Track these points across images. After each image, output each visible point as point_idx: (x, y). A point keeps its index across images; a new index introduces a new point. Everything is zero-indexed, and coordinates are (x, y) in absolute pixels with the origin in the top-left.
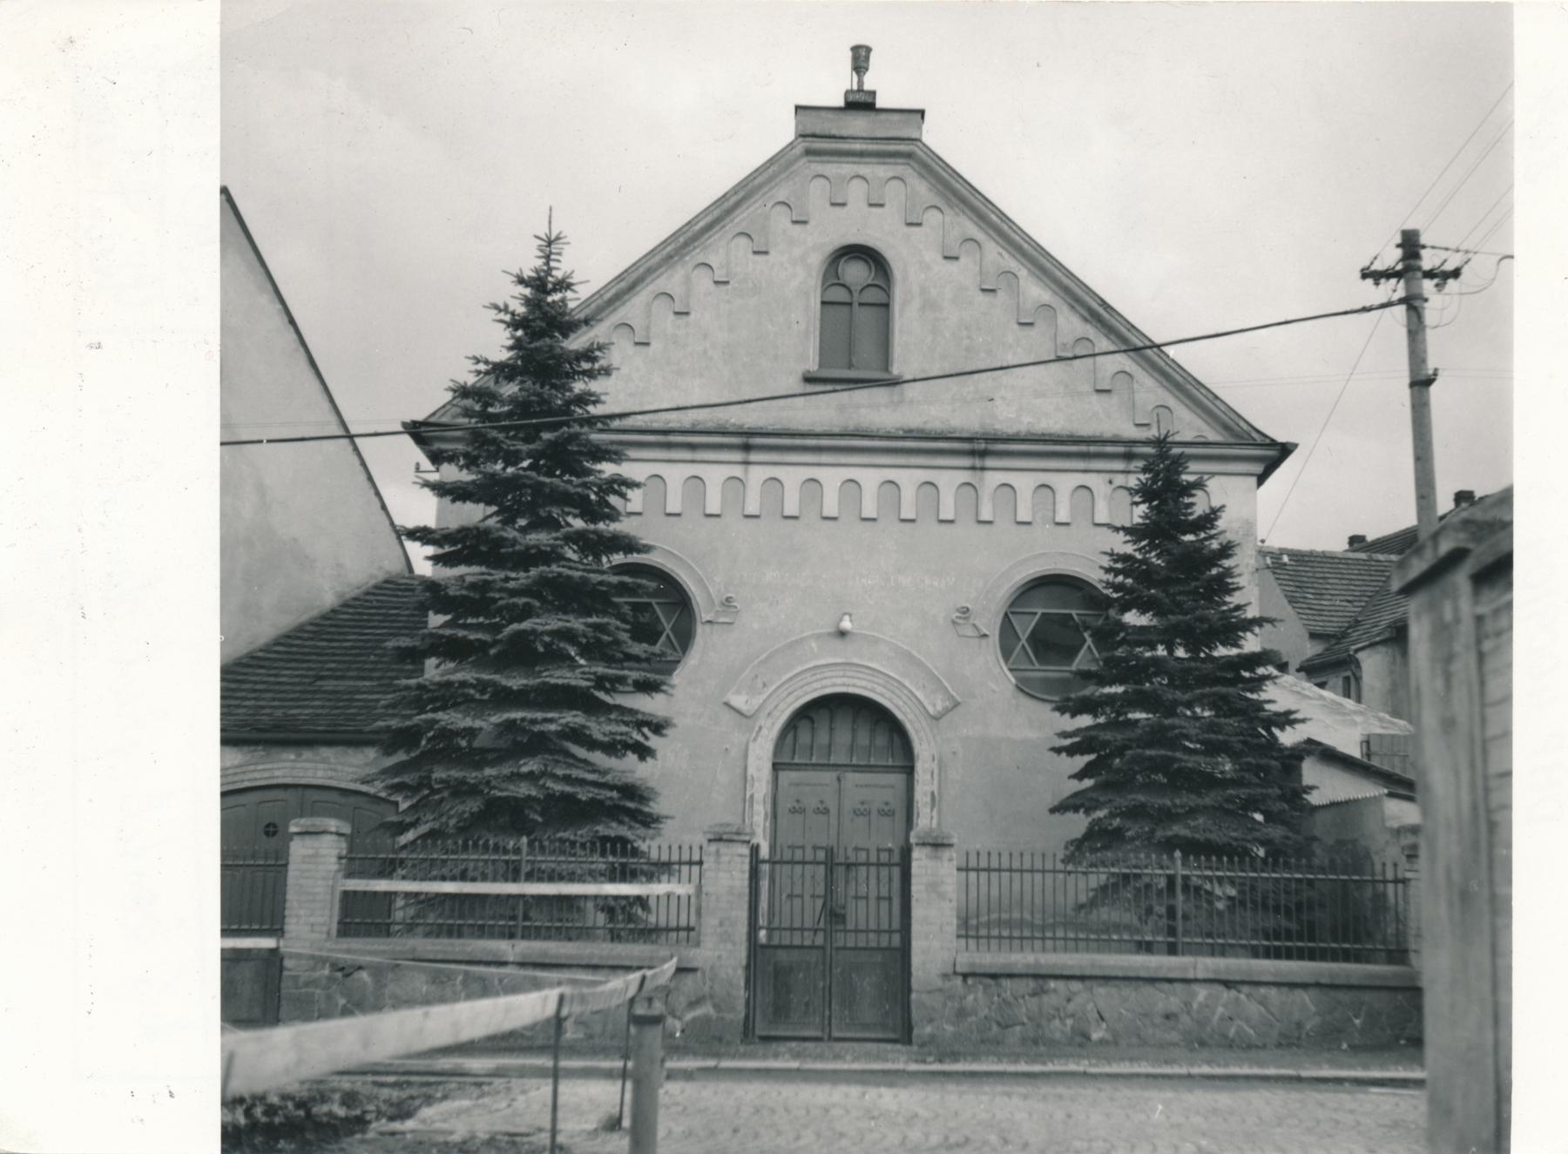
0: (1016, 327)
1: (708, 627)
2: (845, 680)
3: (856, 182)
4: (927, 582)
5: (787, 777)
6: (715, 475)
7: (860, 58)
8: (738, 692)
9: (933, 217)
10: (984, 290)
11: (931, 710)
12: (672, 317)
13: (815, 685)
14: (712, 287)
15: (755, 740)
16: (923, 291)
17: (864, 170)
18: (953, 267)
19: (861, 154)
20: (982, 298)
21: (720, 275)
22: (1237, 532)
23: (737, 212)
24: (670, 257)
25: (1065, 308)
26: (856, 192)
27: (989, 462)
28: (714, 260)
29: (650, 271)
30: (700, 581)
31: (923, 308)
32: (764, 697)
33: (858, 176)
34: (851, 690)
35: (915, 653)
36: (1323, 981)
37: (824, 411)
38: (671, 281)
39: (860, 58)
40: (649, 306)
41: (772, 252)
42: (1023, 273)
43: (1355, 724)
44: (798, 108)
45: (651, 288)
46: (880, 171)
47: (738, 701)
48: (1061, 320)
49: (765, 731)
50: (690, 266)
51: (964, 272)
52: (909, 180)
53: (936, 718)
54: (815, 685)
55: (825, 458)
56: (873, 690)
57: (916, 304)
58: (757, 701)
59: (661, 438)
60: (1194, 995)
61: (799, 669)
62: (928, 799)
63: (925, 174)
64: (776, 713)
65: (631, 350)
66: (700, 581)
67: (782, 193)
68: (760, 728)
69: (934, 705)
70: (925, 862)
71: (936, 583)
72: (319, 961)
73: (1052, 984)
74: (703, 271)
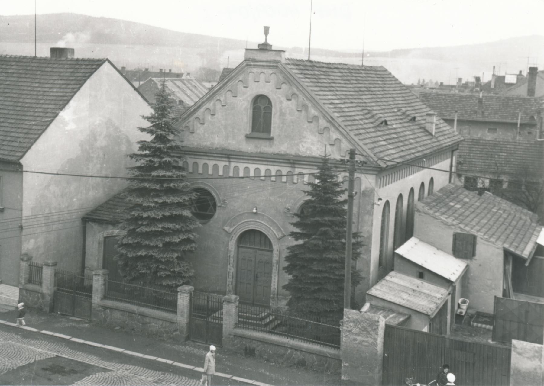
0: (307, 122)
1: (219, 208)
2: (255, 226)
3: (262, 74)
4: (278, 199)
5: (241, 250)
6: (221, 164)
7: (266, 30)
8: (227, 226)
9: (284, 86)
10: (298, 111)
11: (278, 236)
12: (210, 116)
13: (247, 227)
14: (221, 107)
15: (231, 240)
16: (281, 110)
17: (265, 70)
18: (289, 103)
19: (263, 66)
20: (297, 113)
21: (223, 103)
22: (369, 192)
23: (228, 84)
24: (209, 98)
25: (322, 118)
26: (262, 77)
27: (296, 166)
28: (222, 99)
29: (203, 103)
30: (217, 195)
31: (280, 115)
32: (233, 228)
33: (262, 72)
34: (256, 229)
35: (274, 220)
36: (317, 353)
37: (249, 147)
38: (210, 105)
39: (266, 30)
40: (204, 112)
41: (238, 97)
42: (310, 105)
43: (452, 229)
44: (247, 49)
45: (204, 107)
46: (270, 71)
47: (227, 228)
48: (320, 121)
49: (233, 238)
50: (215, 100)
51: (292, 104)
52: (277, 74)
53: (279, 239)
54: (247, 227)
55: (250, 162)
56: (262, 229)
57: (278, 114)
58: (231, 229)
59: (205, 154)
60: (287, 350)
61: (243, 221)
62: (276, 262)
63: (6, 307)
64: (236, 233)
65: (199, 125)
66: (217, 195)
67: (241, 78)
68: (232, 237)
69: (279, 235)
70: (226, 305)
71: (280, 200)
72: (99, 306)
73: (254, 341)
74: (218, 102)
